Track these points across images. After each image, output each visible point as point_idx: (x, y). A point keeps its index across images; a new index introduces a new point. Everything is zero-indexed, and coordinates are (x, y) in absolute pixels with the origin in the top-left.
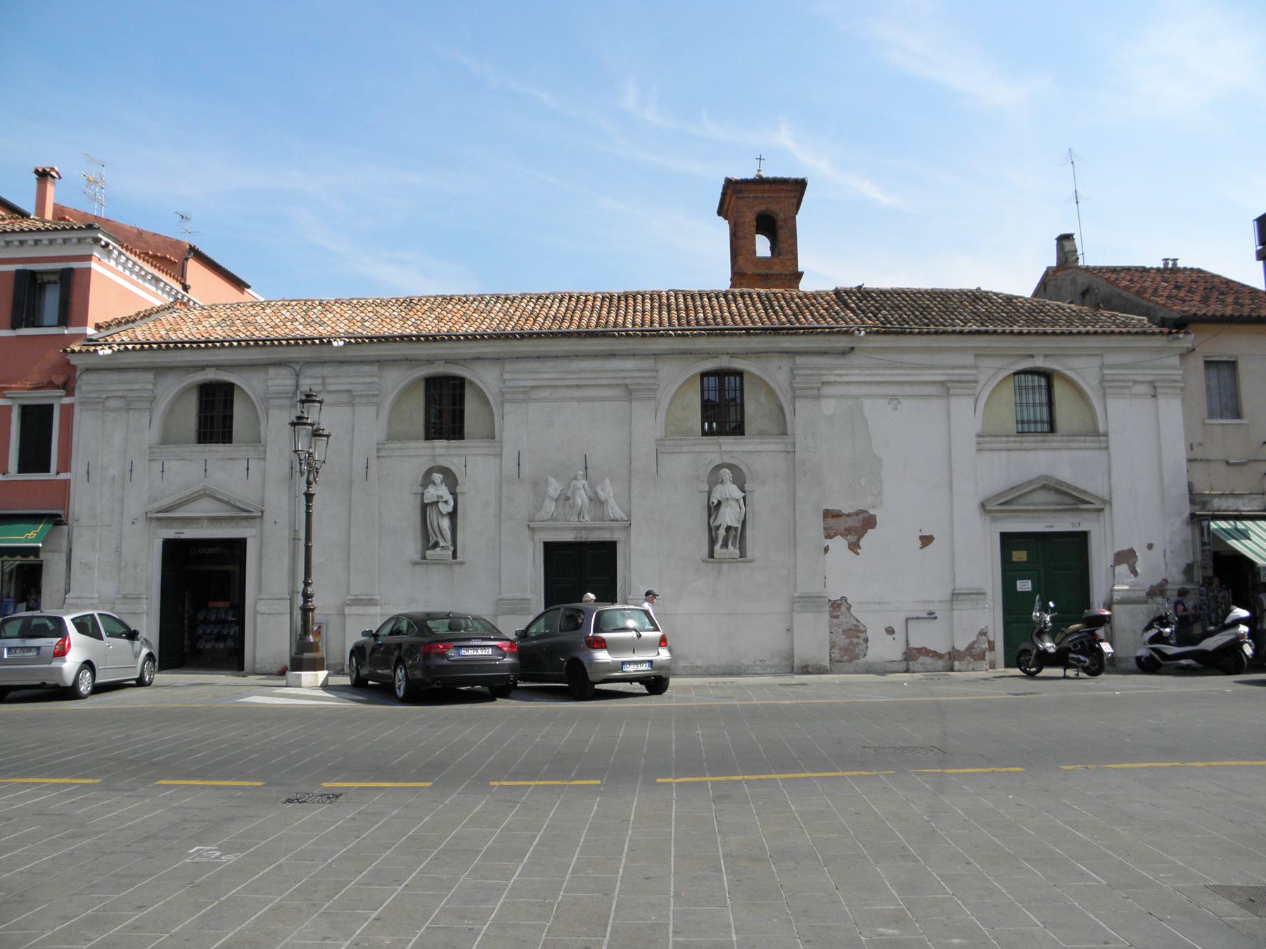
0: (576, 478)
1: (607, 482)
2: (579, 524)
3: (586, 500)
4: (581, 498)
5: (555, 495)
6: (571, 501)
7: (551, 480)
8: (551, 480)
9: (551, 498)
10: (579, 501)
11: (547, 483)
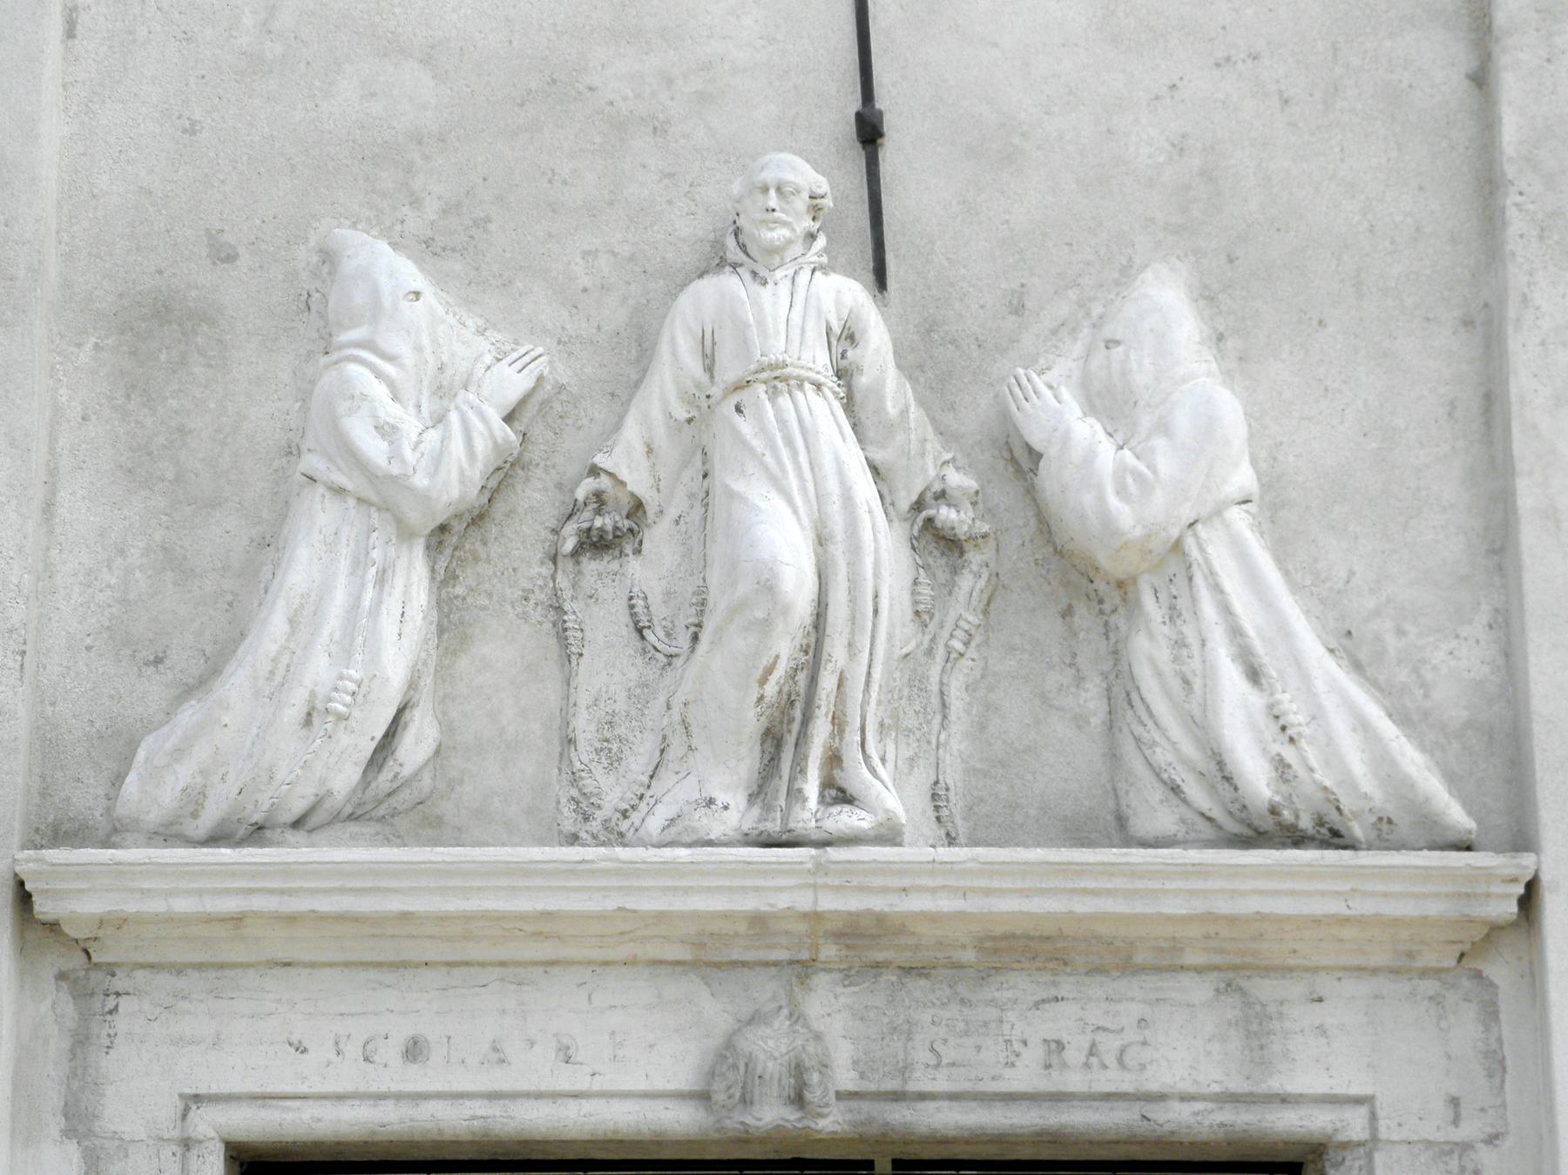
0: (732, 250)
1: (1166, 303)
2: (784, 886)
3: (884, 552)
4: (808, 511)
5: (444, 459)
6: (651, 570)
7: (385, 267)
8: (385, 267)
9: (379, 496)
10: (781, 539)
11: (315, 314)
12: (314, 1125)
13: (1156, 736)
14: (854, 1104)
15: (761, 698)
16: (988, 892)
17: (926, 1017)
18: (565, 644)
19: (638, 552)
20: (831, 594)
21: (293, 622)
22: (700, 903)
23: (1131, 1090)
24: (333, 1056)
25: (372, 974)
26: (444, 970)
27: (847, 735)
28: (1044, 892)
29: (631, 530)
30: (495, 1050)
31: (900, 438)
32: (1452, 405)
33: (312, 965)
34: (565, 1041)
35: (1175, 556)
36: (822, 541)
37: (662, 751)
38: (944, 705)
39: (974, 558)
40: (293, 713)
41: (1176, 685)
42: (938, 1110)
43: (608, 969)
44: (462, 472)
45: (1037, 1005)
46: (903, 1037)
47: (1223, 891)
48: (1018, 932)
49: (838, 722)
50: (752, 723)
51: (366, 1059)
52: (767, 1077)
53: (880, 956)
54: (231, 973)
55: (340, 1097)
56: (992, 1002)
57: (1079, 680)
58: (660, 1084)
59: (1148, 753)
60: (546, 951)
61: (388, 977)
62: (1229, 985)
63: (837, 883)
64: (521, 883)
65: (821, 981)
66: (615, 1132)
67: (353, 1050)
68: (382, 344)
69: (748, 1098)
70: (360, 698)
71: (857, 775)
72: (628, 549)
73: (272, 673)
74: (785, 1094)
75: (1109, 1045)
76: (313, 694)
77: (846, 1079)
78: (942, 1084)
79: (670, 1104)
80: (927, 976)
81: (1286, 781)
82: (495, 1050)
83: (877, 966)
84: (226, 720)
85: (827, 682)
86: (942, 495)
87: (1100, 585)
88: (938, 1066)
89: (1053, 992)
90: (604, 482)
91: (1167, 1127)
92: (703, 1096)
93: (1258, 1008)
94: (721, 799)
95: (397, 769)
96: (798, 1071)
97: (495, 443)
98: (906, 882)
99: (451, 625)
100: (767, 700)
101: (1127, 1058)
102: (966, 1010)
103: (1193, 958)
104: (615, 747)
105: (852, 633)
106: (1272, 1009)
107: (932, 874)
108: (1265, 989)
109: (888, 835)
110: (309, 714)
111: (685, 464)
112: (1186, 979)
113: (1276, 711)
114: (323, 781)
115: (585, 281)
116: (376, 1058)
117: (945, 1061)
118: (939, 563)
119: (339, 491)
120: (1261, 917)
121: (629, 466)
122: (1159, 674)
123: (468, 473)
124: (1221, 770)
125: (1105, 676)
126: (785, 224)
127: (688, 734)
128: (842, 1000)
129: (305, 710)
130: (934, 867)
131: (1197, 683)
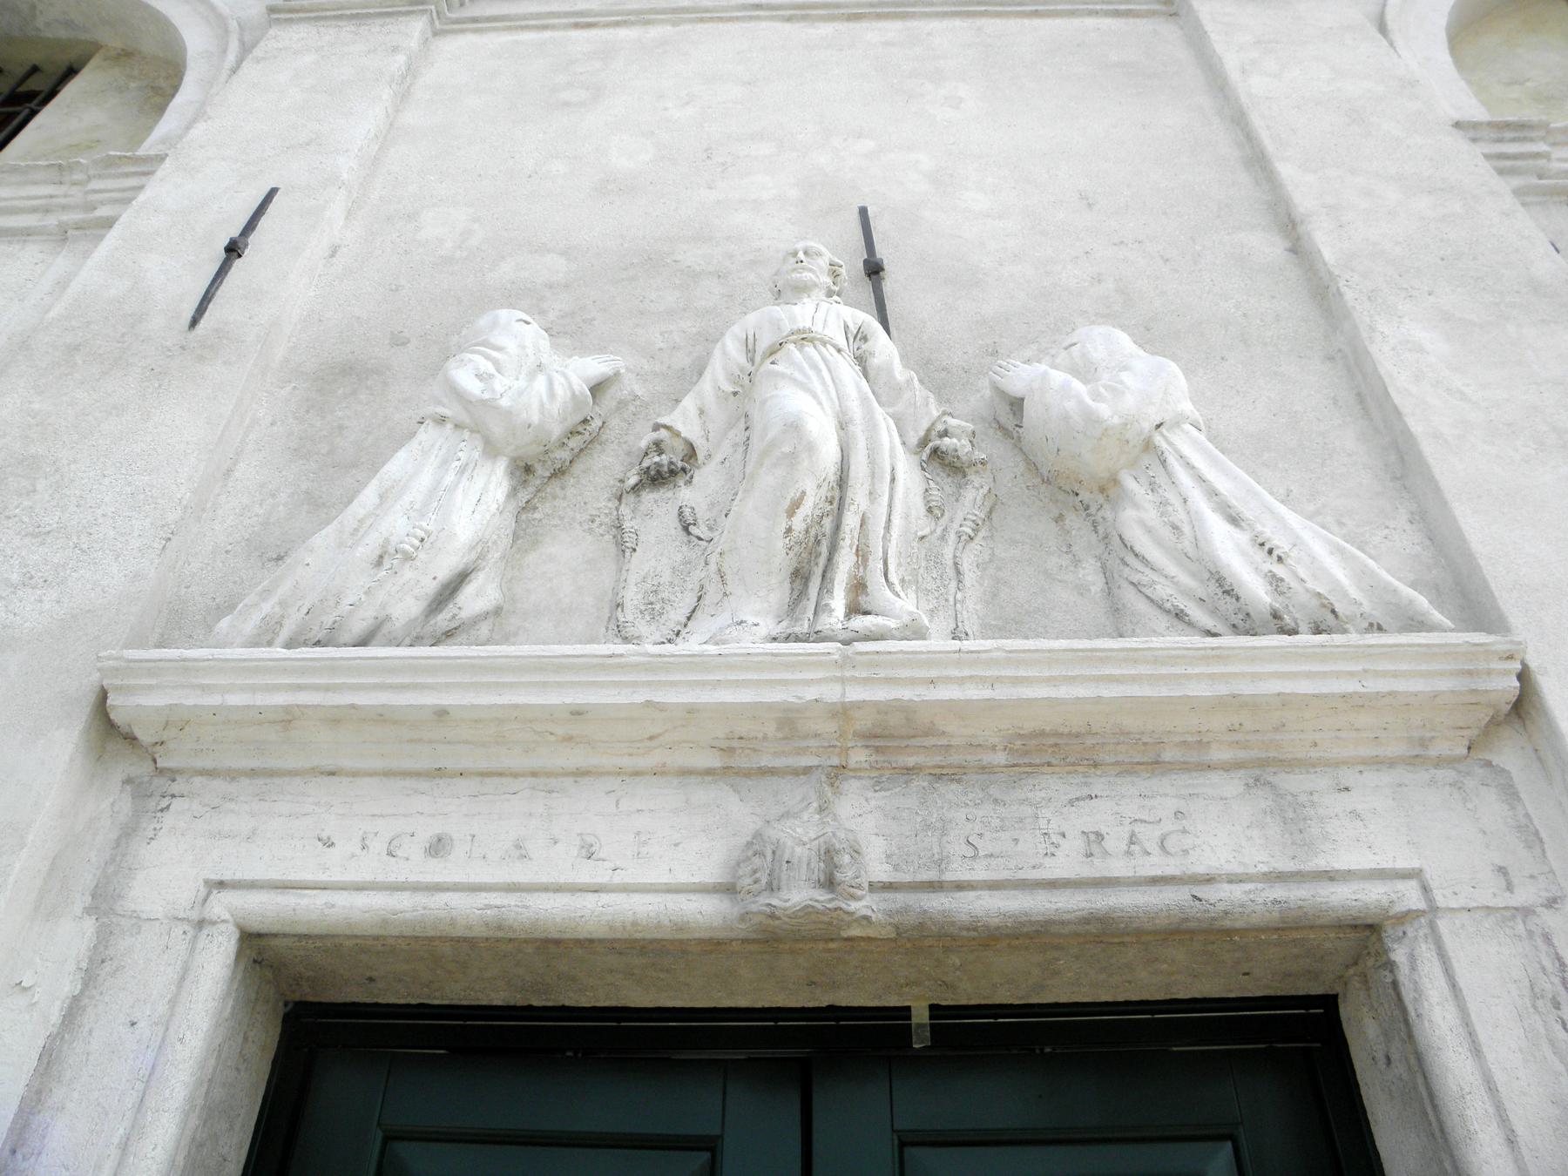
12: (326, 911)
13: (1154, 576)
14: (887, 895)
15: (789, 530)
16: (1017, 681)
17: (960, 815)
18: (623, 546)
19: (689, 482)
20: (852, 461)
21: (382, 497)
22: (726, 696)
23: (1177, 872)
24: (358, 851)
25: (409, 783)
26: (478, 779)
27: (870, 563)
28: (1071, 680)
29: (684, 470)
30: (518, 847)
31: (907, 395)
32: (1335, 401)
33: (355, 774)
34: (590, 839)
35: (1148, 450)
36: (843, 426)
37: (700, 598)
38: (958, 572)
39: (975, 479)
40: (367, 549)
41: (1166, 532)
42: (978, 898)
43: (638, 779)
44: (542, 405)
45: (1071, 803)
46: (937, 833)
47: (1243, 675)
48: (1048, 729)
49: (862, 554)
50: (781, 559)
51: (390, 854)
52: (795, 861)
53: (911, 761)
54: (277, 780)
55: (360, 887)
56: (1023, 802)
57: (1076, 562)
58: (683, 877)
59: (1148, 592)
60: (575, 758)
61: (423, 785)
62: (1257, 780)
63: (864, 675)
64: (552, 678)
65: (852, 786)
66: (635, 924)
67: (377, 846)
68: (492, 340)
69: (775, 883)
70: (427, 545)
71: (879, 592)
72: (681, 483)
73: (356, 530)
74: (815, 877)
75: (1150, 836)
76: (387, 540)
77: (880, 871)
78: (980, 873)
79: (693, 897)
80: (959, 781)
81: (1282, 593)
82: (518, 847)
83: (909, 771)
84: (308, 560)
85: (851, 521)
86: (945, 433)
87: (1085, 495)
88: (974, 857)
89: (1086, 791)
90: (663, 433)
91: (1221, 907)
92: (728, 889)
93: (1289, 798)
94: (751, 619)
95: (455, 611)
96: (829, 855)
97: (574, 396)
98: (933, 673)
99: (525, 526)
100: (795, 534)
101: (1169, 844)
102: (1001, 810)
103: (1219, 754)
104: (657, 607)
105: (873, 484)
106: (1303, 798)
107: (959, 664)
108: (1292, 782)
109: (915, 631)
110: (381, 557)
111: (731, 426)
112: (1215, 777)
113: (1260, 540)
114: (383, 606)
115: (661, 345)
116: (399, 853)
117: (981, 853)
118: (948, 483)
119: (441, 420)
120: (1284, 701)
121: (685, 420)
122: (1149, 531)
123: (547, 406)
124: (1221, 586)
125: (1099, 558)
126: (810, 270)
127: (724, 583)
128: (873, 803)
129: (378, 553)
130: (960, 658)
131: (1186, 529)
